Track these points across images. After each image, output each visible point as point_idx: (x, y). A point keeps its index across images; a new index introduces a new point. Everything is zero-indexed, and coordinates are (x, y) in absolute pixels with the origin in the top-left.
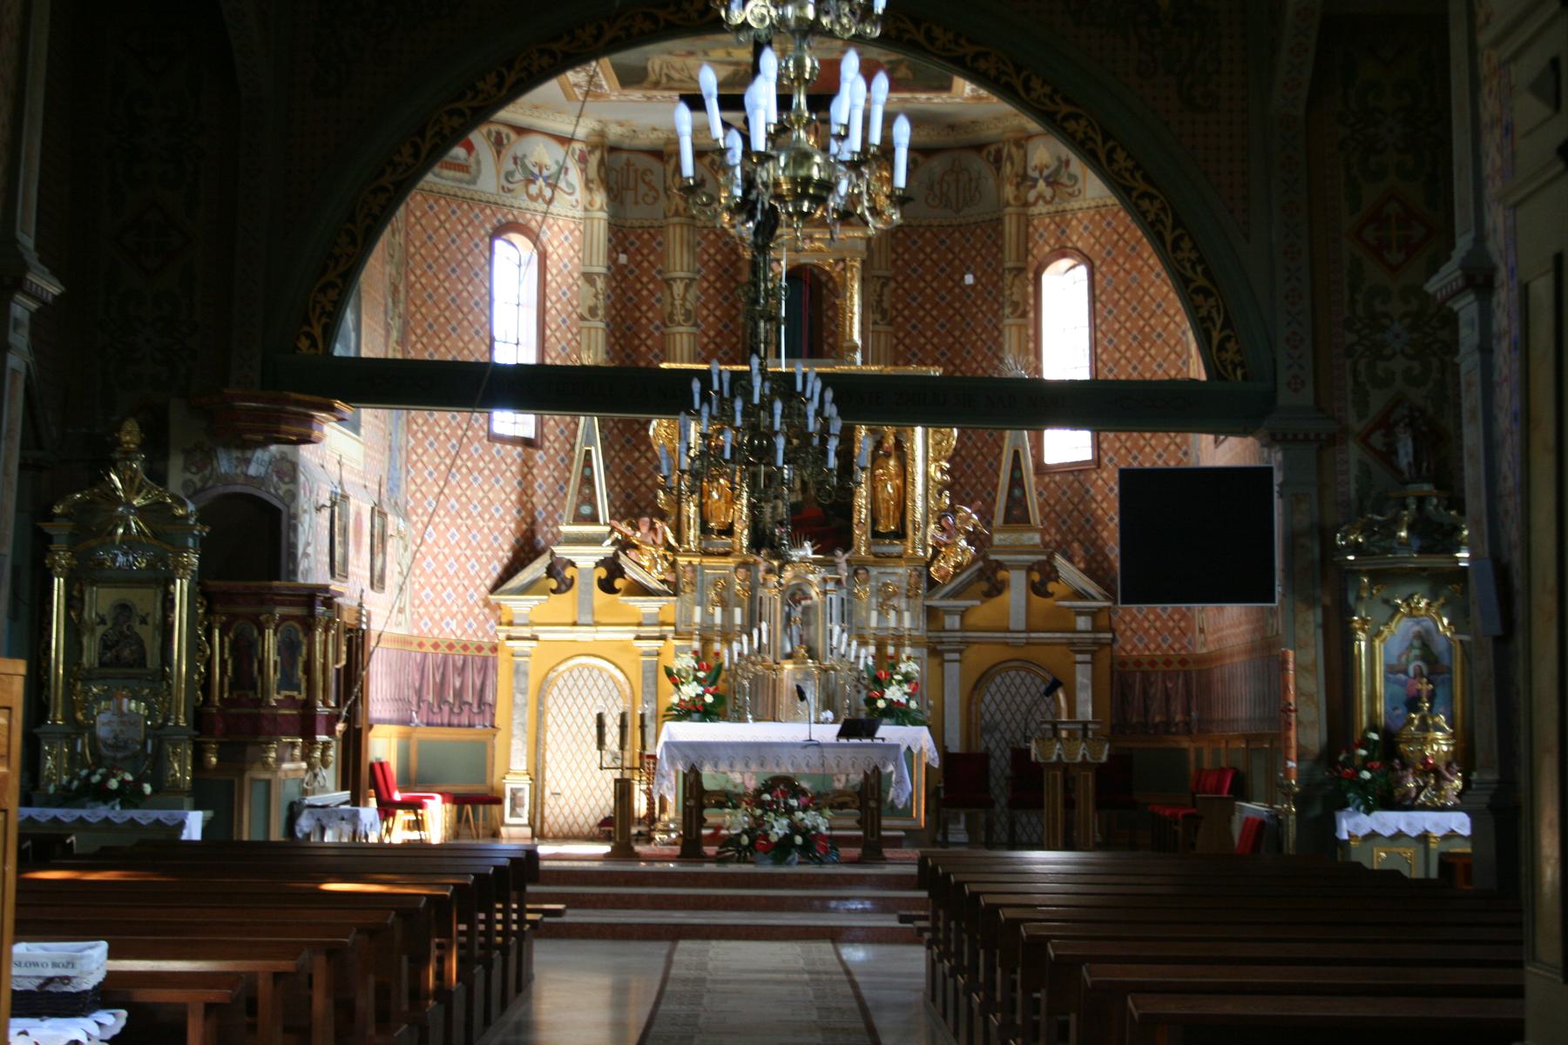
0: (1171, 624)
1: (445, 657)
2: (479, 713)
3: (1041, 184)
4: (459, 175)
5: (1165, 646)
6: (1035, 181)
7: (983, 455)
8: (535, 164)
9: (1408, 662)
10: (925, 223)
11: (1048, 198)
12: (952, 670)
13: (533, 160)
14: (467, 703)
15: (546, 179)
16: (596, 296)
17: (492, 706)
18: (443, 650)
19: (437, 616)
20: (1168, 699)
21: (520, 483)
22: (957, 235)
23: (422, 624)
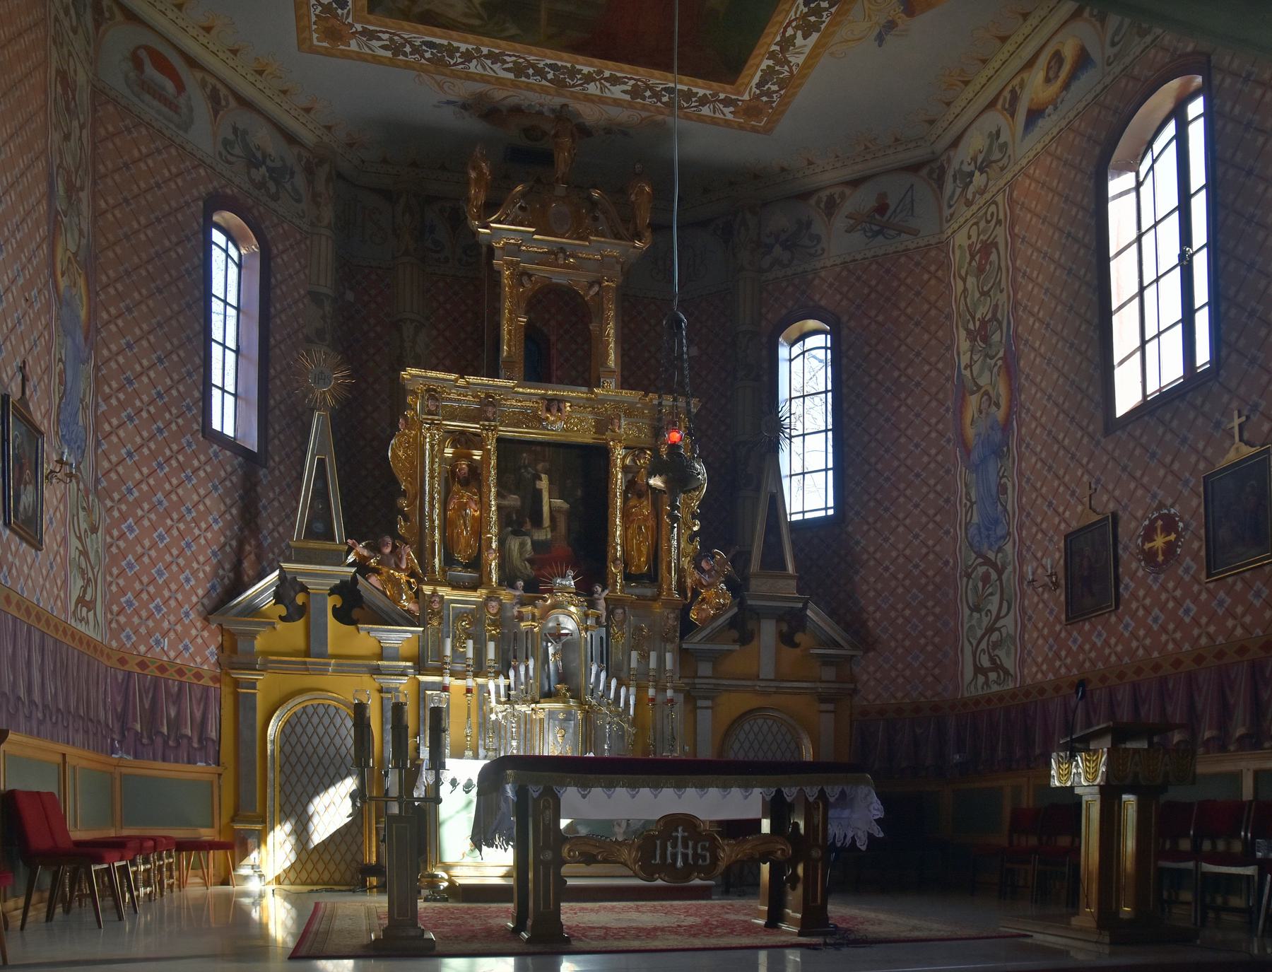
2: (200, 749)
3: (778, 250)
4: (165, 109)
8: (259, 148)
12: (705, 718)
14: (186, 736)
18: (152, 671)
19: (143, 630)
21: (241, 497)
23: (123, 636)
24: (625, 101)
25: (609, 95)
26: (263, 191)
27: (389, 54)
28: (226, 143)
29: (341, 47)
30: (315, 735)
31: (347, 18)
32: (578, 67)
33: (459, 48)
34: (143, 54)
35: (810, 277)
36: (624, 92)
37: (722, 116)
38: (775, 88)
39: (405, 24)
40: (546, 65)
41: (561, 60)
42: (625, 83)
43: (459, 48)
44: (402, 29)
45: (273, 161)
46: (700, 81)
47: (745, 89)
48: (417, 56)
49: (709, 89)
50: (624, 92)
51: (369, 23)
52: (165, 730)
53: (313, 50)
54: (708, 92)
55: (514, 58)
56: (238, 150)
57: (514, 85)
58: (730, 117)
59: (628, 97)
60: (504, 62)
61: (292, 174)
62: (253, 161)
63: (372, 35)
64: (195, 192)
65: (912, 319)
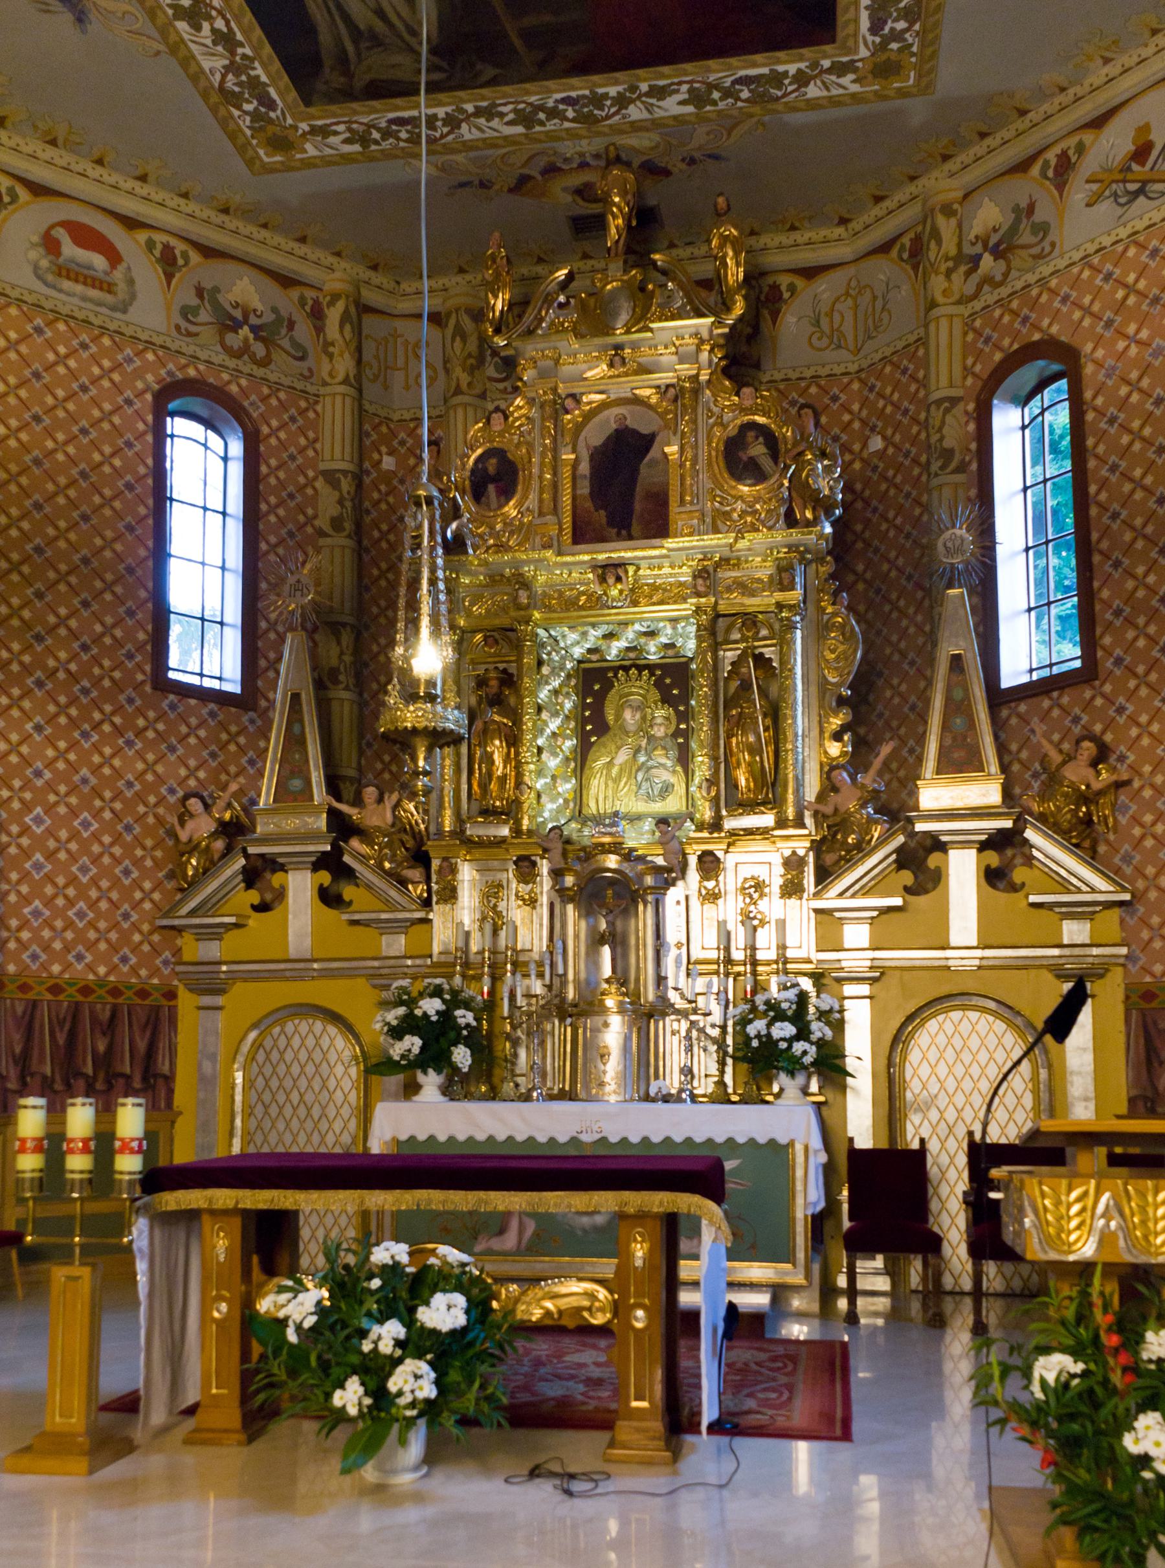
1: (76, 1008)
6: (976, 260)
7: (900, 695)
8: (236, 306)
10: (808, 373)
11: (998, 278)
13: (231, 297)
14: (123, 1075)
15: (255, 329)
16: (341, 502)
17: (169, 1079)
18: (71, 995)
19: (57, 945)
22: (856, 386)
24: (690, 114)
25: (661, 113)
26: (246, 357)
27: (357, 148)
28: (187, 312)
29: (298, 156)
30: (296, 1063)
31: (285, 119)
32: (601, 91)
33: (787, 72)
34: (61, 234)
35: (1035, 292)
36: (681, 103)
37: (841, 91)
38: (901, 25)
39: (355, 105)
40: (556, 101)
41: (573, 88)
42: (677, 91)
43: (787, 72)
44: (355, 113)
45: (259, 317)
46: (781, 54)
47: (856, 42)
48: (730, 100)
49: (801, 59)
50: (681, 103)
51: (314, 118)
52: (89, 1070)
53: (269, 170)
54: (802, 65)
55: (511, 107)
56: (204, 316)
57: (880, 96)
58: (855, 88)
59: (690, 109)
60: (502, 115)
61: (291, 325)
62: (228, 323)
63: (325, 132)
64: (140, 385)
65: (300, 453)
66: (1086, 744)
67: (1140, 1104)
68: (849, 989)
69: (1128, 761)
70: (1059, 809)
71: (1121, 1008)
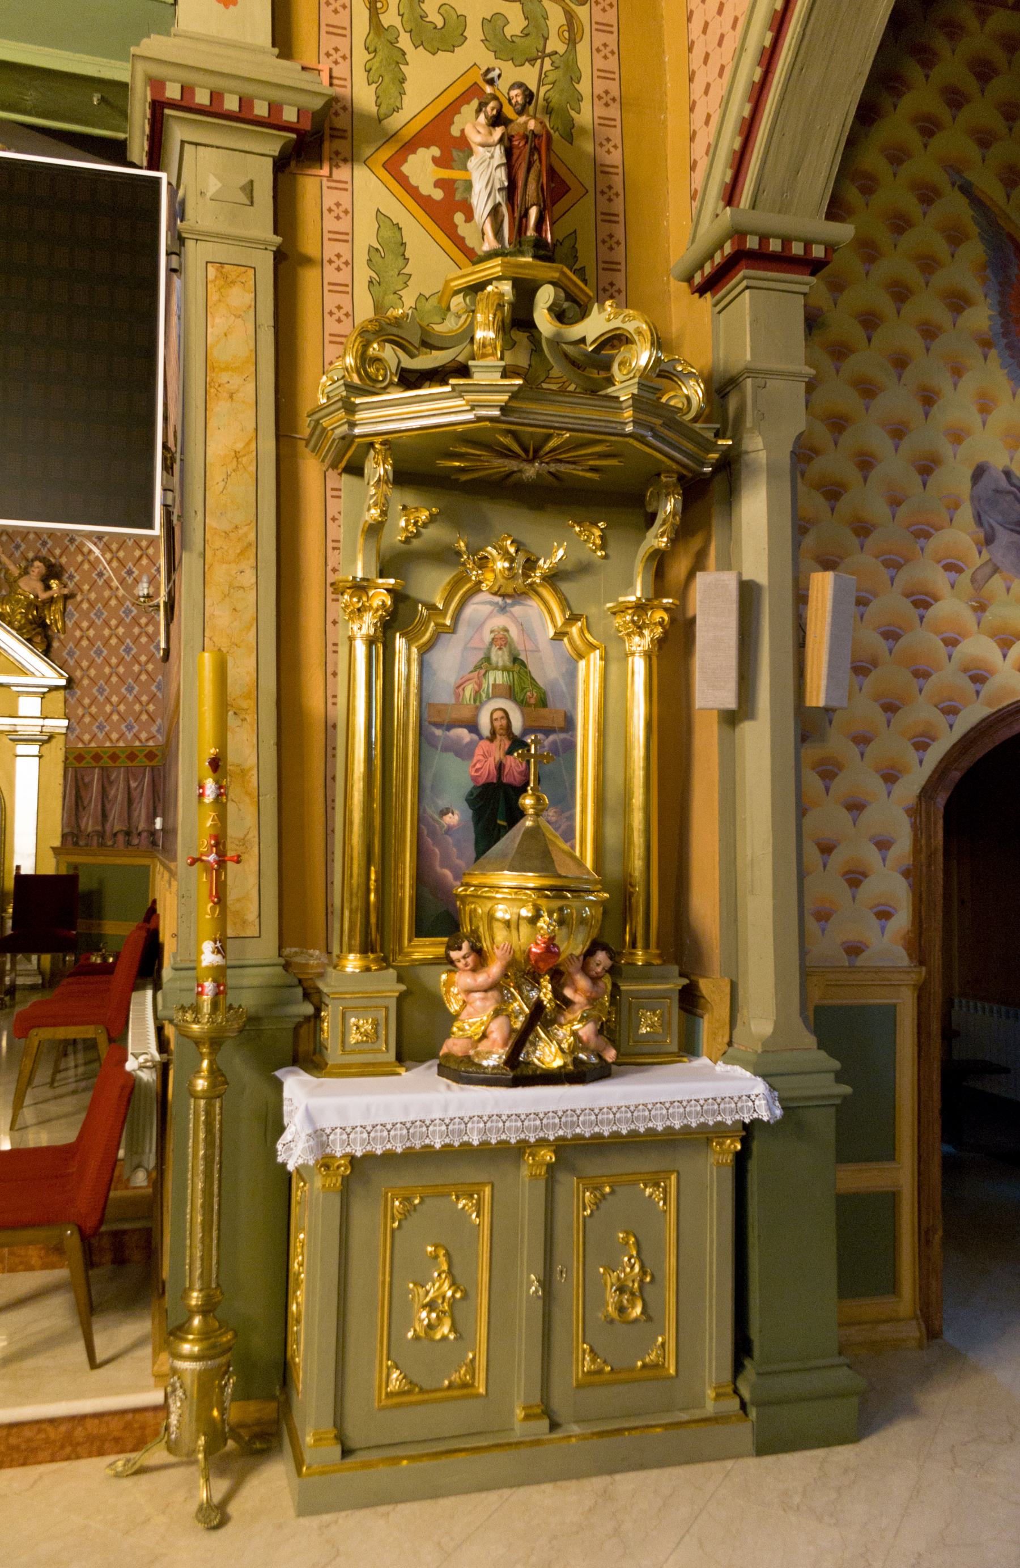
0: (137, 707)
5: (129, 736)
9: (478, 701)
20: (130, 801)
66: (37, 563)
67: (70, 838)
68: (21, 749)
69: (75, 580)
70: (12, 610)
71: (60, 767)
